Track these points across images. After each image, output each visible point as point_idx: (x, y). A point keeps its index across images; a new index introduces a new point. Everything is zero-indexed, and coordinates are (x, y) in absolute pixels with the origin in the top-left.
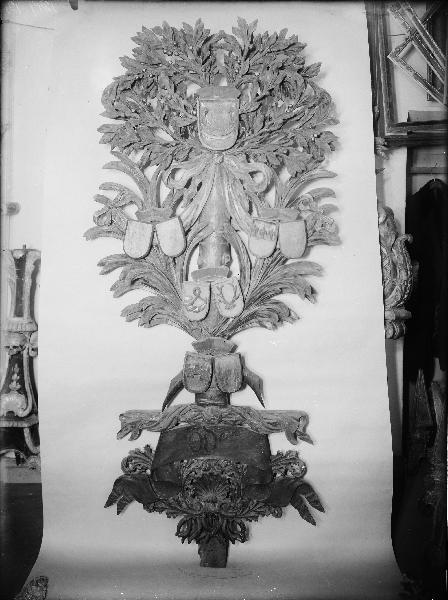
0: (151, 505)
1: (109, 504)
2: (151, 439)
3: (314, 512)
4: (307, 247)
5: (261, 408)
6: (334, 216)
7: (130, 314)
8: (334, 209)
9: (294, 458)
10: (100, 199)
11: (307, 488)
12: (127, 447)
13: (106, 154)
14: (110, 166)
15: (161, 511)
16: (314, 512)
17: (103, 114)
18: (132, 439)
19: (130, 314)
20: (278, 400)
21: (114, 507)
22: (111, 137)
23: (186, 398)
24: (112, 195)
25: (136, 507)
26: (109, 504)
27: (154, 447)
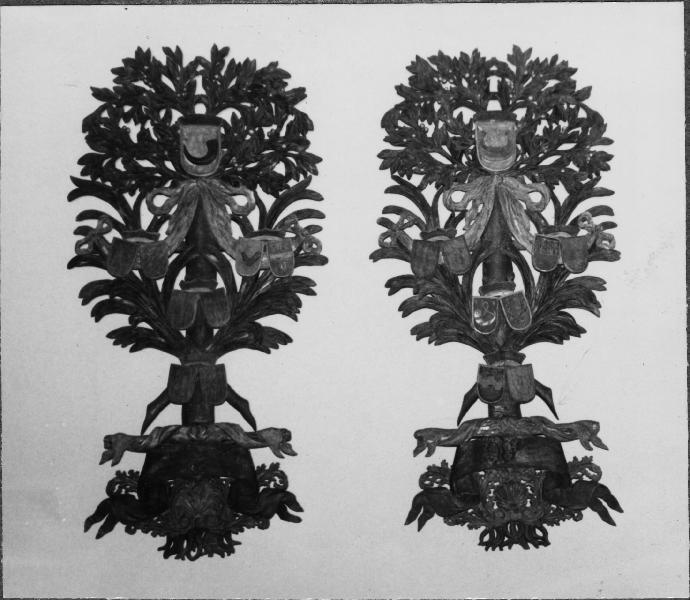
0: (453, 517)
1: (409, 520)
2: (446, 455)
3: (612, 513)
4: (474, 263)
5: (247, 428)
6: (316, 236)
7: (419, 332)
8: (318, 229)
9: (588, 462)
10: (383, 222)
11: (605, 492)
12: (423, 463)
13: (386, 179)
14: (390, 190)
15: (463, 523)
16: (612, 513)
17: (386, 140)
18: (113, 465)
19: (419, 332)
20: (568, 413)
21: (415, 523)
22: (388, 160)
23: (480, 410)
24: (93, 223)
25: (437, 521)
26: (409, 520)
27: (450, 462)
